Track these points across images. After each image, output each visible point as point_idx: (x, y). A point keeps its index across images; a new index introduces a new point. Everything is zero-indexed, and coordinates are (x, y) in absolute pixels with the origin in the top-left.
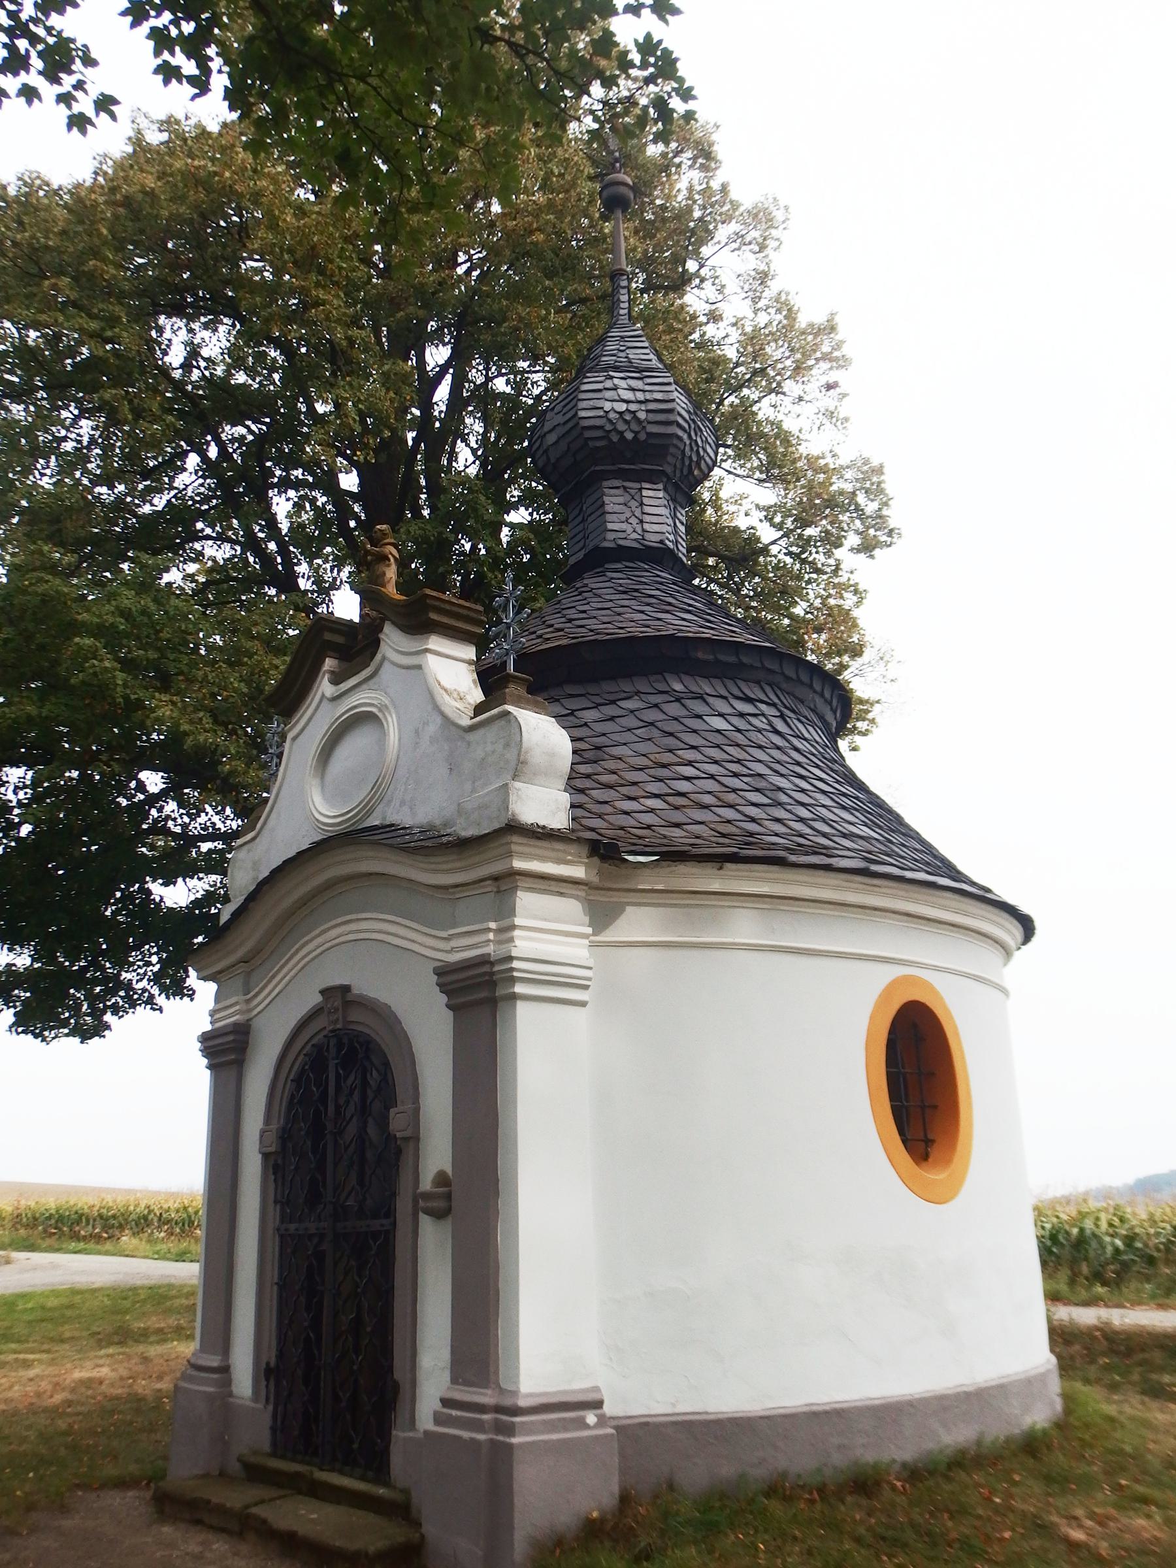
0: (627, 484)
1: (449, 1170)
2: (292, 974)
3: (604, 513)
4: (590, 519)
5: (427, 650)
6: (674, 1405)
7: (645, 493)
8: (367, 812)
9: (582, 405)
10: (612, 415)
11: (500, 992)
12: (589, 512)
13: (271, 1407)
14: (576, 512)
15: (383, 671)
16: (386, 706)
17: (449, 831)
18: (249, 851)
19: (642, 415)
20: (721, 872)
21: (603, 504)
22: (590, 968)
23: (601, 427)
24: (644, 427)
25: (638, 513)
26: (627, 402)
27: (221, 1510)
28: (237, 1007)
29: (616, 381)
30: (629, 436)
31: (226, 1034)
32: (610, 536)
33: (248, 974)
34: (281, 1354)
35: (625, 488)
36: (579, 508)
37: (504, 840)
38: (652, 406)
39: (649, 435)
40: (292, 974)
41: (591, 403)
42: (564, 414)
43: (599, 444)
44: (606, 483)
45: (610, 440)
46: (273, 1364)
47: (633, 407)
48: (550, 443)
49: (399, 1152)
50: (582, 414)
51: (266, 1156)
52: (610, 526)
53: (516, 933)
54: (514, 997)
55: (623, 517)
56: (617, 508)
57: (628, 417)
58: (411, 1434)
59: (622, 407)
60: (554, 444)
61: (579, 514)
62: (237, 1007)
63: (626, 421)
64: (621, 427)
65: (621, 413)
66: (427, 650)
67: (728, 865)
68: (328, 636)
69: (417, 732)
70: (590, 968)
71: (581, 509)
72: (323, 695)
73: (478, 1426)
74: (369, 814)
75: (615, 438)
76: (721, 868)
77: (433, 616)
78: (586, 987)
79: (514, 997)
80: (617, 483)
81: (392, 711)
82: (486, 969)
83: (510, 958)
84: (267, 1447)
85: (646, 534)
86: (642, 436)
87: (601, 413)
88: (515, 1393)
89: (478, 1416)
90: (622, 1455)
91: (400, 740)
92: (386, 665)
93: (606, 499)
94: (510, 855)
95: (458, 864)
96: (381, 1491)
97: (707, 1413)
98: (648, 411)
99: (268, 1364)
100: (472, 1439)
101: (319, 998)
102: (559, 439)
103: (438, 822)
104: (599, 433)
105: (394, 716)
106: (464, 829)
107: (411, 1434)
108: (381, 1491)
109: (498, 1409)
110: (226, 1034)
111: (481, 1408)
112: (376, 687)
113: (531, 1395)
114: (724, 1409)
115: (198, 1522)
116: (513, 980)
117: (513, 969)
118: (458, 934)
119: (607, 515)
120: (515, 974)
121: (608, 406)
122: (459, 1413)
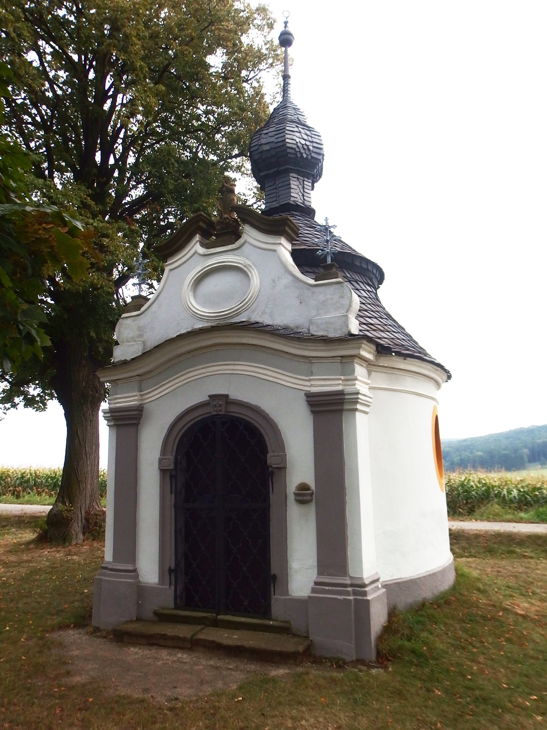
0: (299, 177)
1: (311, 482)
2: (179, 384)
3: (290, 188)
4: (280, 189)
5: (280, 244)
6: (392, 576)
7: (305, 183)
8: (236, 314)
9: (287, 136)
10: (299, 144)
11: (346, 407)
12: (280, 185)
13: (173, 587)
14: (272, 183)
15: (244, 248)
16: (249, 265)
17: (300, 330)
18: (133, 321)
19: (311, 148)
20: (405, 361)
21: (290, 184)
22: (371, 398)
23: (294, 149)
24: (311, 154)
25: (302, 191)
26: (305, 140)
27: (184, 639)
28: (136, 398)
29: (300, 129)
30: (305, 156)
31: (134, 410)
32: (292, 199)
33: (140, 382)
34: (177, 564)
35: (298, 179)
36: (274, 182)
37: (361, 342)
38: (315, 145)
39: (312, 157)
40: (179, 384)
41: (291, 136)
42: (277, 138)
43: (292, 156)
44: (291, 175)
45: (297, 155)
46: (173, 567)
47: (308, 143)
48: (265, 149)
49: (272, 474)
50: (287, 140)
51: (163, 471)
52: (292, 194)
53: (357, 382)
54: (356, 410)
55: (297, 191)
56: (295, 187)
57: (306, 147)
58: (288, 597)
59: (303, 142)
60: (268, 150)
61: (273, 185)
62: (136, 398)
63: (304, 149)
64: (302, 151)
65: (303, 145)
66: (280, 244)
67: (408, 358)
68: (201, 224)
69: (274, 281)
70: (371, 398)
71: (275, 183)
72: (196, 252)
73: (348, 593)
74: (237, 315)
75: (299, 155)
76: (405, 359)
77: (287, 229)
78: (368, 406)
79: (356, 410)
80: (295, 175)
81: (254, 268)
82: (342, 397)
83: (358, 393)
84: (172, 605)
85: (305, 201)
86: (309, 157)
87: (295, 142)
88: (362, 578)
89: (345, 589)
90: (388, 598)
91: (261, 283)
92: (247, 245)
93: (291, 182)
94: (359, 348)
95: (325, 348)
96: (271, 623)
97: (402, 578)
98: (313, 147)
99: (170, 568)
100: (345, 599)
101: (208, 398)
102: (271, 149)
103: (292, 326)
104: (293, 151)
105: (256, 271)
106: (316, 332)
107: (288, 597)
108: (271, 623)
109: (352, 585)
110: (134, 410)
111: (345, 586)
112: (239, 254)
113: (368, 578)
114: (407, 576)
115: (153, 645)
116: (357, 402)
117: (358, 398)
118: (320, 379)
119: (292, 190)
120: (359, 400)
121: (298, 140)
122: (330, 588)
